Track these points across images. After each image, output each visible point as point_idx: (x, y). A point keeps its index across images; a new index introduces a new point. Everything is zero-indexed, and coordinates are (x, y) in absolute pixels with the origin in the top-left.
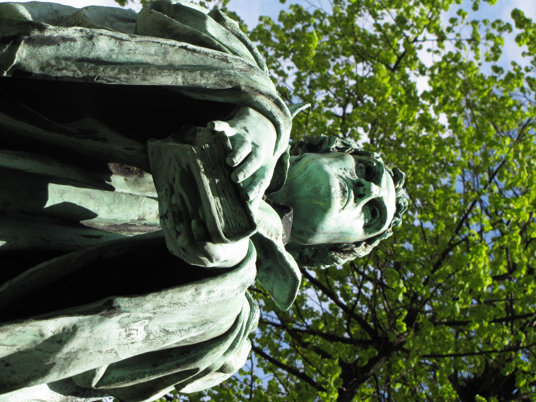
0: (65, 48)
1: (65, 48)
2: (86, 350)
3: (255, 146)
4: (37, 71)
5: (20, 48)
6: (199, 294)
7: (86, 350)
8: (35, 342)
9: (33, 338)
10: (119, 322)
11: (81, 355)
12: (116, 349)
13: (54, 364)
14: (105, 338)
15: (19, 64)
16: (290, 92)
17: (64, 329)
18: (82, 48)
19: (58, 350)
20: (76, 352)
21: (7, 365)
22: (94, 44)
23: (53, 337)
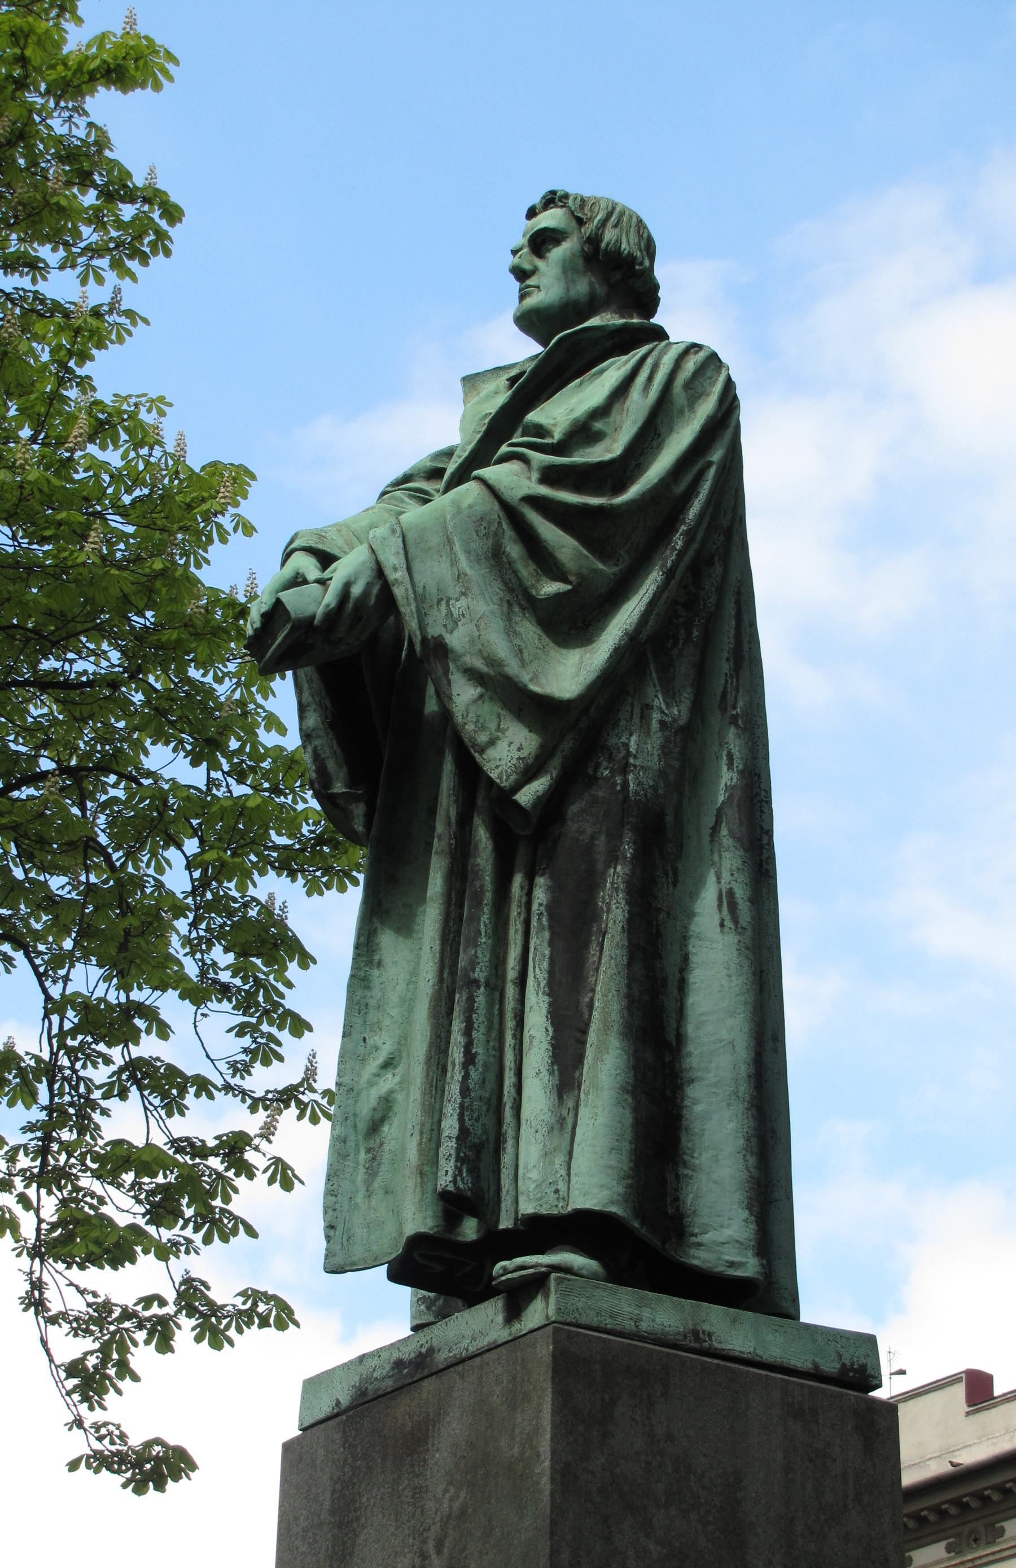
0: (324, 752)
1: (324, 752)
2: (480, 651)
3: (532, 213)
4: (345, 769)
5: (335, 791)
6: (396, 580)
7: (480, 651)
8: (491, 698)
9: (487, 702)
10: (452, 632)
11: (485, 654)
12: (475, 622)
13: (499, 674)
14: (467, 639)
15: (347, 786)
16: (203, 665)
17: (470, 680)
18: (319, 737)
19: (488, 675)
20: (484, 659)
21: (521, 710)
22: (314, 730)
23: (482, 686)
